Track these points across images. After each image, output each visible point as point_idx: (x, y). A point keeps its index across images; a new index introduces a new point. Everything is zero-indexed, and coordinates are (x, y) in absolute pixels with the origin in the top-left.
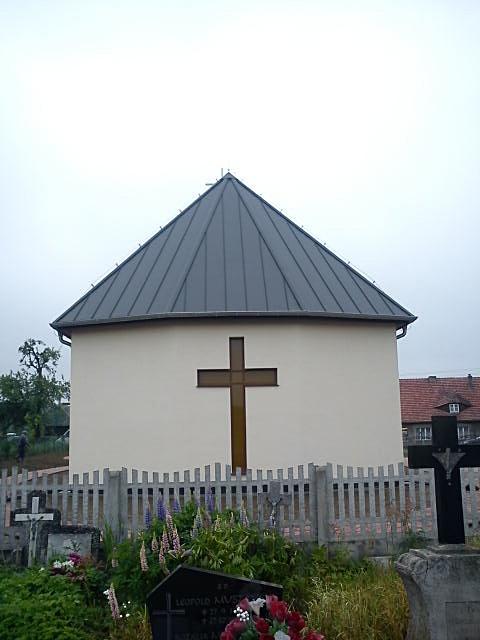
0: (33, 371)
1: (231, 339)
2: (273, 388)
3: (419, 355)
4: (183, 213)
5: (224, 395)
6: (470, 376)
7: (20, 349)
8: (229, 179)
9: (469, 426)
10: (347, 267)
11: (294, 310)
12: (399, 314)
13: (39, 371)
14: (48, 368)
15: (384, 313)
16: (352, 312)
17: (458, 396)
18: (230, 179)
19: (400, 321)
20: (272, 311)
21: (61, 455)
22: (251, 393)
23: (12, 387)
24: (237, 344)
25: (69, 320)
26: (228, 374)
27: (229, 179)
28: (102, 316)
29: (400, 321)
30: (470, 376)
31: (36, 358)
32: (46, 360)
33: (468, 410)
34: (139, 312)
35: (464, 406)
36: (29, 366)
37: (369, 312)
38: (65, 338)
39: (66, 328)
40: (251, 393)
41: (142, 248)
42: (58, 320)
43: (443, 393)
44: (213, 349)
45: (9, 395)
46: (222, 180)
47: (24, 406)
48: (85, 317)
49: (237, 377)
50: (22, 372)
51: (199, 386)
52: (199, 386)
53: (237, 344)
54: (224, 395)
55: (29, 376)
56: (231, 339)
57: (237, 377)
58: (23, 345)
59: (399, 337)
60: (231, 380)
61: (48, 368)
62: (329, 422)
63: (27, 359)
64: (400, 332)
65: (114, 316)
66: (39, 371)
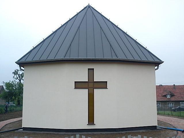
0: (18, 81)
1: (88, 69)
2: (106, 89)
3: (164, 77)
4: (70, 20)
5: (85, 92)
6: (174, 85)
7: (13, 73)
8: (89, 7)
9: (160, 103)
10: (135, 41)
11: (114, 58)
12: (156, 60)
13: (20, 81)
14: (23, 80)
15: (151, 59)
16: (130, 58)
17: (170, 92)
18: (89, 7)
19: (156, 63)
20: (88, 58)
21: (20, 114)
22: (97, 92)
23: (10, 87)
24: (91, 72)
25: (23, 60)
26: (87, 83)
27: (89, 8)
28: (37, 59)
29: (156, 63)
30: (174, 85)
31: (19, 76)
32: (22, 77)
33: (173, 97)
34: (51, 58)
35: (172, 95)
36: (16, 79)
37: (144, 59)
38: (22, 68)
39: (21, 63)
40: (97, 92)
41: (54, 33)
42: (18, 61)
43: (165, 91)
44: (81, 73)
45: (9, 89)
46: (86, 7)
47: (14, 93)
48: (29, 59)
49: (91, 85)
50: (14, 81)
51: (75, 88)
52: (75, 88)
53: (91, 72)
54: (85, 92)
55: (16, 83)
56: (88, 69)
57: (91, 85)
58: (14, 71)
59: (156, 69)
60: (88, 86)
61: (23, 80)
62: (127, 101)
63: (16, 76)
64: (156, 68)
65: (34, 60)
66: (20, 81)
